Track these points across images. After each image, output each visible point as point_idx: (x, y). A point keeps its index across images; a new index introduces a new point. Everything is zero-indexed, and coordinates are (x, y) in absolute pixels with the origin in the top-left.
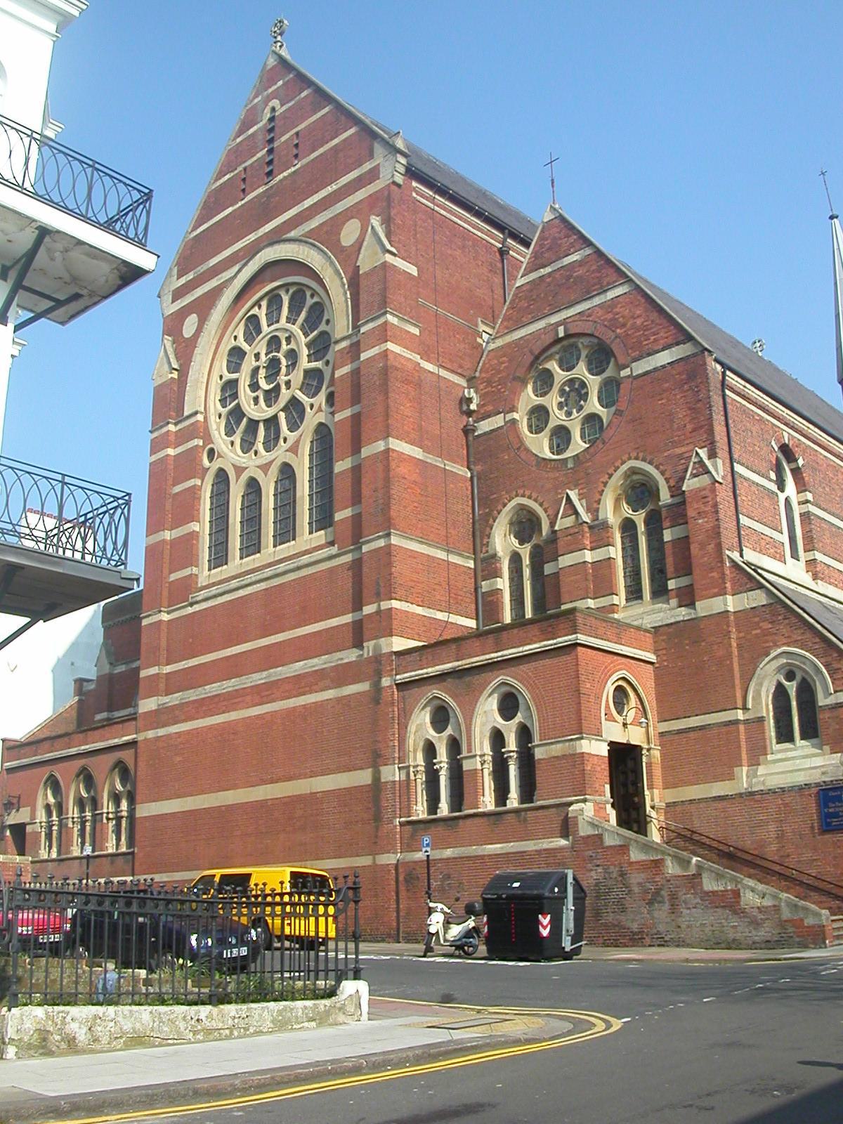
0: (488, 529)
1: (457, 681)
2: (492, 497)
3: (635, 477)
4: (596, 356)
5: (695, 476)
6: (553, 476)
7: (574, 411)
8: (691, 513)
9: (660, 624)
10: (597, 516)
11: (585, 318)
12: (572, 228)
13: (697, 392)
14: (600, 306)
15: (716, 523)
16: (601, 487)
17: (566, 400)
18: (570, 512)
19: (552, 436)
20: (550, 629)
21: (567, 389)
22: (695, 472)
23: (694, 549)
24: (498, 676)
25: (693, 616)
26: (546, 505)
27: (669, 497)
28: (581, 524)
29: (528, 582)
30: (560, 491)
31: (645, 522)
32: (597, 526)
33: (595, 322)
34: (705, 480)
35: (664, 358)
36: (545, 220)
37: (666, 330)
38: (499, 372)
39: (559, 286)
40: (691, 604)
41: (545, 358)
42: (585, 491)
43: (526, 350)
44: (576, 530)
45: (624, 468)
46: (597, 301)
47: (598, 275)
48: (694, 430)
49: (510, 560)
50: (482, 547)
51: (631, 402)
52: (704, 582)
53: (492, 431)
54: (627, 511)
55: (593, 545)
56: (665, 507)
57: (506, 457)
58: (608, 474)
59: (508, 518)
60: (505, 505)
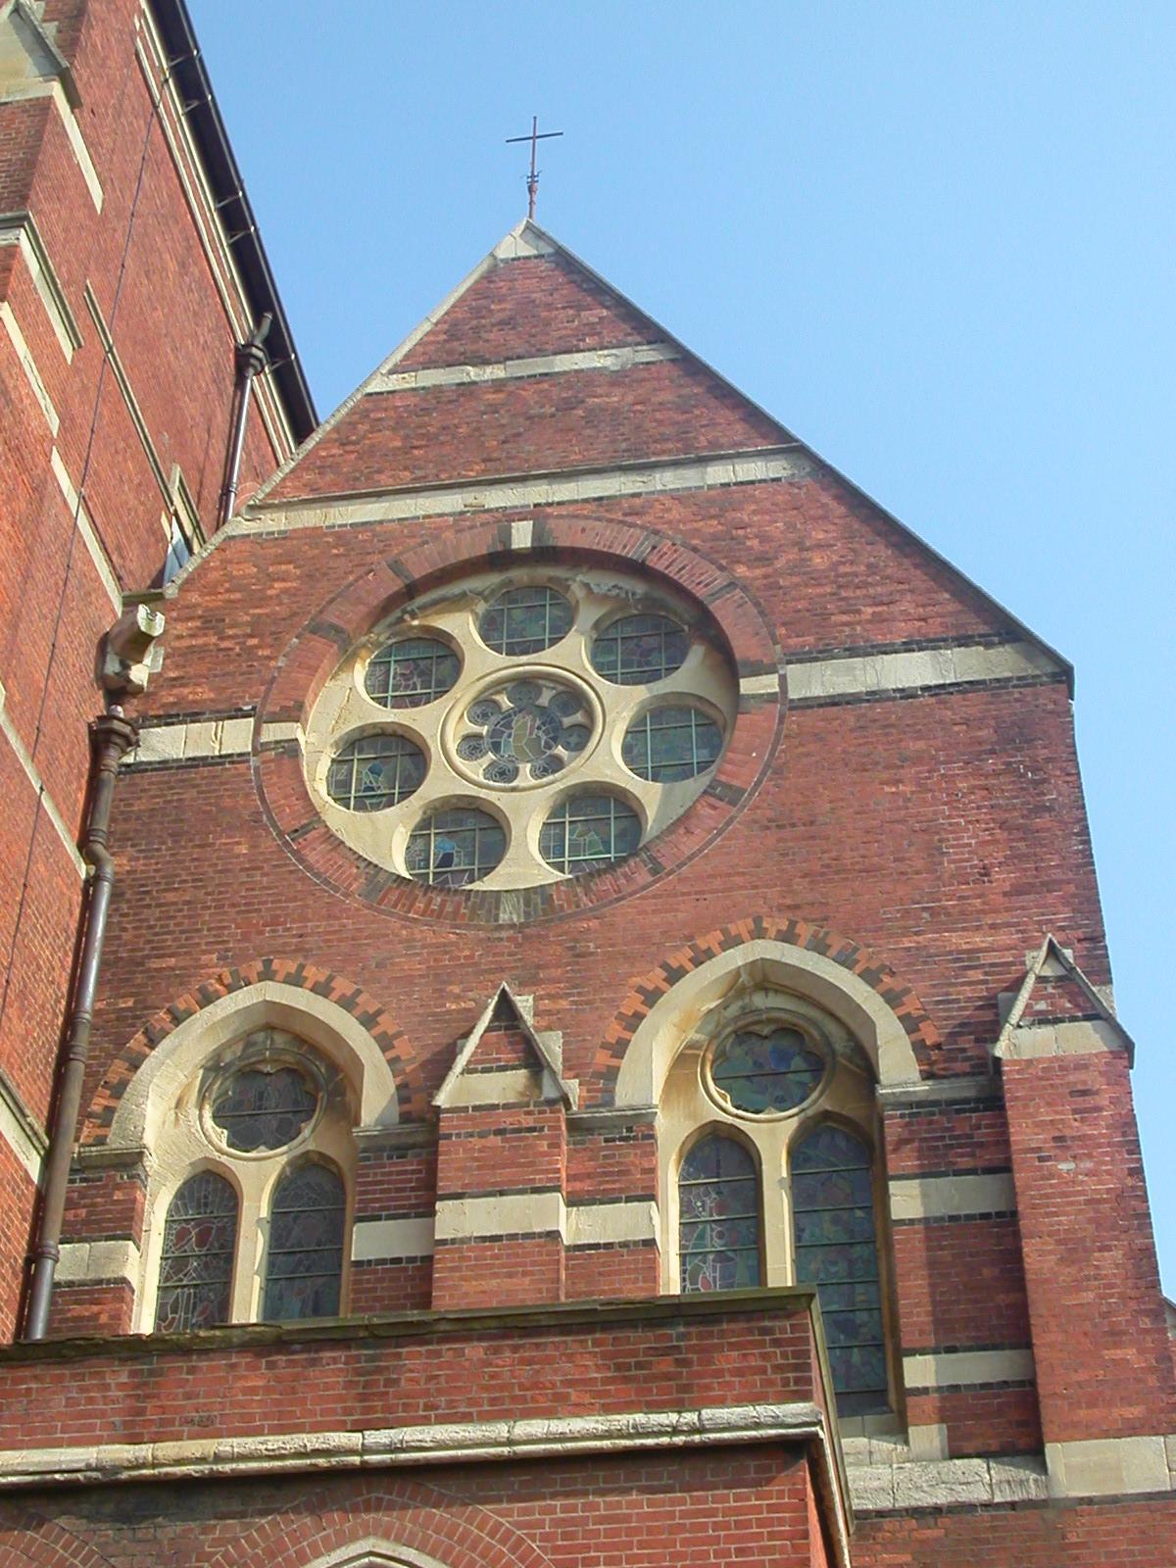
0: (119, 1067)
1: (108, 1531)
2: (155, 964)
3: (760, 1001)
4: (629, 632)
5: (1043, 1020)
6: (431, 939)
7: (526, 768)
8: (1024, 1133)
9: (885, 1503)
10: (610, 1092)
11: (619, 516)
12: (597, 289)
13: (1036, 783)
14: (678, 497)
15: (1130, 1182)
16: (632, 1003)
17: (493, 733)
18: (507, 1057)
19: (425, 824)
20: (666, 1365)
21: (505, 702)
22: (1042, 1006)
23: (1039, 1257)
24: (354, 1538)
25: (1034, 1492)
26: (386, 1023)
27: (916, 1076)
28: (550, 1102)
29: (257, 1281)
30: (456, 989)
31: (790, 1153)
32: (604, 1125)
33: (656, 532)
34: (1083, 1039)
35: (912, 670)
36: (501, 254)
37: (922, 599)
38: (262, 600)
39: (530, 418)
40: (1030, 1450)
41: (435, 603)
42: (564, 1004)
43: (376, 558)
44: (528, 1121)
45: (736, 958)
46: (667, 480)
47: (681, 418)
48: (1018, 890)
49: (180, 1195)
50: (81, 1123)
51: (775, 770)
52: (1082, 1376)
53: (195, 763)
54: (716, 1105)
55: (578, 1186)
56: (898, 1105)
57: (244, 849)
58: (665, 966)
59: (210, 1046)
60: (207, 999)
